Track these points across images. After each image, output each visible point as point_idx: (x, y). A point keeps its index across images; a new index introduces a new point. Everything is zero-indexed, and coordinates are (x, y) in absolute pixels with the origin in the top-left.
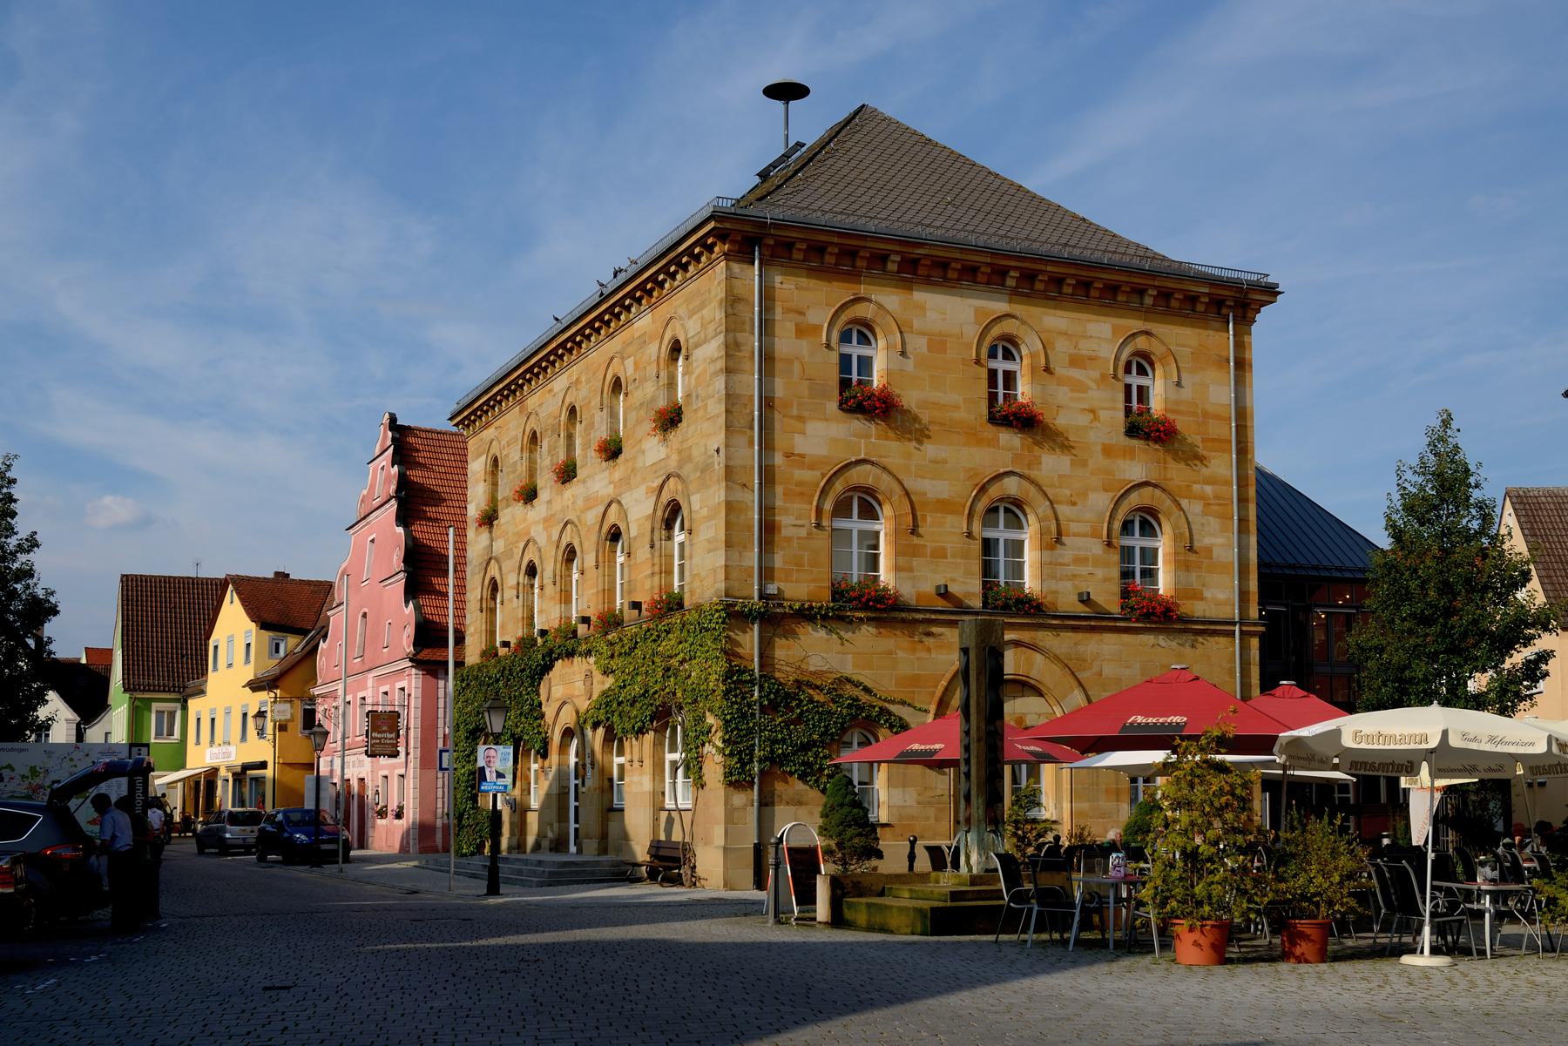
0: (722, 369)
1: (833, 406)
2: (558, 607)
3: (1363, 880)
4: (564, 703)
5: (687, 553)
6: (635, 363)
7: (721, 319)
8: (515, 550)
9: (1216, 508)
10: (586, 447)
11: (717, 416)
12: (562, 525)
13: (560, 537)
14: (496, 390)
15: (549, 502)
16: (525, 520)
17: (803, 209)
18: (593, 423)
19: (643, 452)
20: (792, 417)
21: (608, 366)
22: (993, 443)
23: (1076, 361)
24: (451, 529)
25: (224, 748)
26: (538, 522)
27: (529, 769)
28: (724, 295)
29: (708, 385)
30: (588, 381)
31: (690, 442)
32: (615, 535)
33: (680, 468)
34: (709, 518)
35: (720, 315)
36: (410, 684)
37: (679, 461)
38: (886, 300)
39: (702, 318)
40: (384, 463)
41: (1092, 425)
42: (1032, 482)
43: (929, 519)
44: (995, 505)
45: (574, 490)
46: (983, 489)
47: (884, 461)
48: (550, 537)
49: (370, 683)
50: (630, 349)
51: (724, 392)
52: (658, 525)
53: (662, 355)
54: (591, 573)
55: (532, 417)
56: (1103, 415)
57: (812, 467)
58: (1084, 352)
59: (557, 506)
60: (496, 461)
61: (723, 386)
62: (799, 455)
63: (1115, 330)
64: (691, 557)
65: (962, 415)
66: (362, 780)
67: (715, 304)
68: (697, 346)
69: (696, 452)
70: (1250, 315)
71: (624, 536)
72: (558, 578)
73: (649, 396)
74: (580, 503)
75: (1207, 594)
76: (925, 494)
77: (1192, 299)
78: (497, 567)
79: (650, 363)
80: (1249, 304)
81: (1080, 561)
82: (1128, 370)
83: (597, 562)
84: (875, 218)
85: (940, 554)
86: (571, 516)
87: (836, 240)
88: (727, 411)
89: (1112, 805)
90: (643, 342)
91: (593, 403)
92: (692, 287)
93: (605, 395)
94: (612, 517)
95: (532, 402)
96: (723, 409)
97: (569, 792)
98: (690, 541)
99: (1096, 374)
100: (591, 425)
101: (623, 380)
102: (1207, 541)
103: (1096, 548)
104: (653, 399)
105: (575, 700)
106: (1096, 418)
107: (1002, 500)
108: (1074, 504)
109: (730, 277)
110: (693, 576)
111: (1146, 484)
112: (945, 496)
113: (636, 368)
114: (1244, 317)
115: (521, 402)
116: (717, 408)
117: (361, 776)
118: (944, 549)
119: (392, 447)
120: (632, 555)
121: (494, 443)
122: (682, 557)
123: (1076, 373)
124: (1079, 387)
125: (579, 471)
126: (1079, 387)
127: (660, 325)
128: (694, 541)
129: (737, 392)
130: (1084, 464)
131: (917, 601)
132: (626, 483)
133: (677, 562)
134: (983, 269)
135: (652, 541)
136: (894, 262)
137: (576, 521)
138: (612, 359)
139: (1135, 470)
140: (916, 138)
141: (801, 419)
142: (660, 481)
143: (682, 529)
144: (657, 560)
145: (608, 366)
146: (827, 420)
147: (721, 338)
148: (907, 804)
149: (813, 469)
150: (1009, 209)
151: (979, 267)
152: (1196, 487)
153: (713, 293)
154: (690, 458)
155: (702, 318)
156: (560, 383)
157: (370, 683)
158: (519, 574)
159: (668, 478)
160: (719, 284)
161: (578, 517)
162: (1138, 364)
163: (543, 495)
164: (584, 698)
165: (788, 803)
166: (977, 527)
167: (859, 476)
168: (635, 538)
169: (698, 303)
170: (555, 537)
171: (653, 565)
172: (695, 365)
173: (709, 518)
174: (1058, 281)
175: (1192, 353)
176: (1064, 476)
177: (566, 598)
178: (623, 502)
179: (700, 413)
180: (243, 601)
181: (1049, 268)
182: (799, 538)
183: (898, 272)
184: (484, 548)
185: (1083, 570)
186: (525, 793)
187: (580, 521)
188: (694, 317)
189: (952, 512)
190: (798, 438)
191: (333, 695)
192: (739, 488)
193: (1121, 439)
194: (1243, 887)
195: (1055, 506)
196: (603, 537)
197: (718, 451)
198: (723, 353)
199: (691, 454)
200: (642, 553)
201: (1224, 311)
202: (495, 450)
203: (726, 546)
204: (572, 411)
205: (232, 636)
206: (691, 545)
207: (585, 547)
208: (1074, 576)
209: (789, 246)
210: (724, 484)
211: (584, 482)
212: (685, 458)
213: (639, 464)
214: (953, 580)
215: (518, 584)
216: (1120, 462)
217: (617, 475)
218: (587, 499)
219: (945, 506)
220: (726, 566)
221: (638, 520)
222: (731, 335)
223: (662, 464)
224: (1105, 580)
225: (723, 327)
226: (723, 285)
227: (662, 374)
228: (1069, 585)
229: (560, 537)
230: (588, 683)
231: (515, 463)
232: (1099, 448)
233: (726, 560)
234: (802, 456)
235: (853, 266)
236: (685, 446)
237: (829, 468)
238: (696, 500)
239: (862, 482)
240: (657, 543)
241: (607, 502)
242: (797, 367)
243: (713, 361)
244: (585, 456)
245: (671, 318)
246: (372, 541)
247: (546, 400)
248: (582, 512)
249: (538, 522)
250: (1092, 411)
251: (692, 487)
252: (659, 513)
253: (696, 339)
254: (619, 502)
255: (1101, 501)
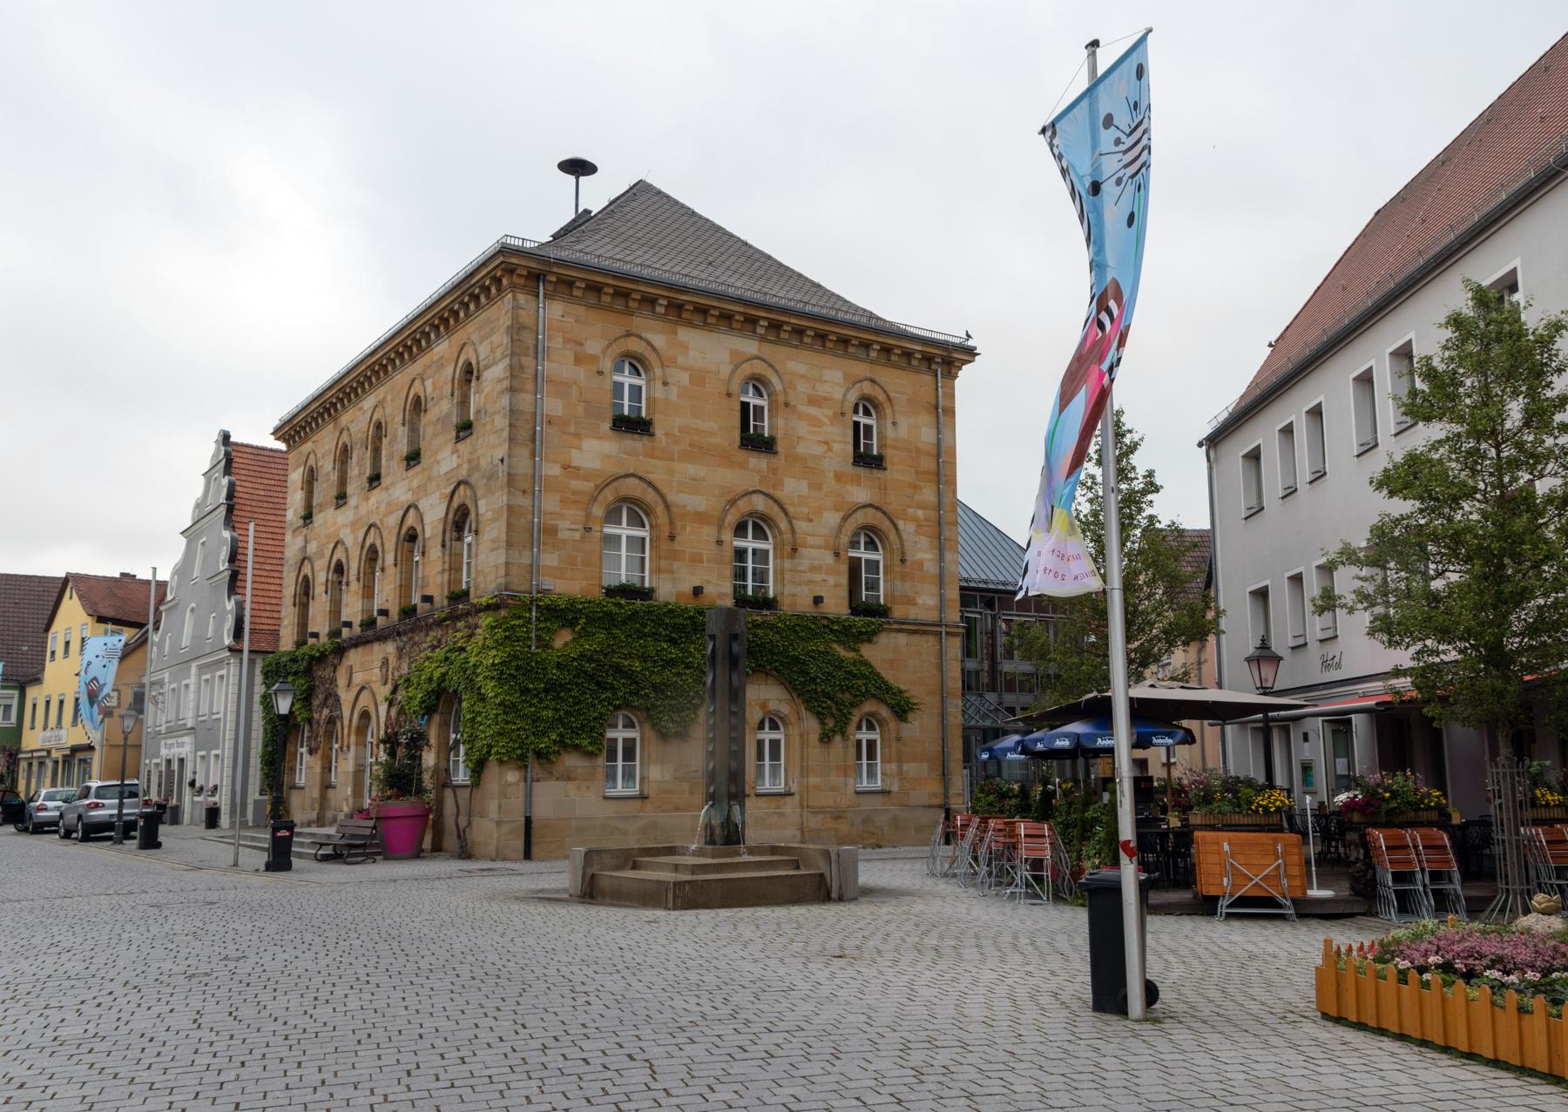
0: (506, 389)
1: (606, 426)
2: (360, 601)
3: (1473, 655)
4: (363, 688)
5: (473, 552)
6: (433, 384)
7: (507, 344)
8: (326, 551)
9: (927, 529)
10: (391, 457)
11: (502, 430)
12: (365, 529)
13: (365, 539)
14: (313, 407)
15: (357, 507)
16: (335, 523)
17: (587, 254)
18: (396, 437)
19: (438, 462)
20: (569, 434)
21: (410, 387)
22: (743, 466)
23: (814, 401)
24: (252, 526)
25: (56, 732)
26: (346, 525)
27: (331, 749)
28: (510, 322)
29: (496, 402)
30: (393, 400)
31: (479, 453)
32: (412, 537)
33: (469, 476)
34: (493, 520)
35: (506, 340)
36: (228, 671)
37: (469, 470)
38: (656, 335)
39: (492, 343)
40: (217, 475)
41: (827, 455)
42: (776, 501)
43: (688, 529)
44: (745, 519)
45: (376, 496)
46: (733, 502)
47: (650, 477)
48: (356, 538)
49: (194, 670)
50: (430, 371)
51: (508, 408)
52: (449, 528)
53: (457, 376)
54: (391, 570)
55: (345, 433)
56: (836, 447)
57: (586, 478)
58: (820, 393)
59: (363, 510)
60: (312, 470)
61: (508, 402)
62: (575, 467)
63: (846, 376)
64: (477, 555)
65: (717, 440)
66: (181, 761)
67: (502, 330)
68: (487, 367)
69: (484, 462)
70: (953, 371)
71: (420, 538)
72: (362, 575)
73: (444, 412)
74: (383, 508)
75: (920, 601)
76: (685, 506)
77: (908, 354)
78: (309, 567)
79: (446, 383)
80: (953, 362)
81: (815, 569)
82: (856, 411)
83: (396, 560)
84: (649, 266)
85: (696, 559)
86: (375, 519)
87: (611, 282)
88: (511, 425)
89: (841, 780)
90: (440, 365)
91: (397, 419)
92: (483, 316)
93: (407, 412)
94: (411, 519)
95: (345, 419)
96: (507, 423)
97: (364, 771)
98: (477, 540)
99: (830, 413)
100: (394, 439)
101: (423, 399)
102: (919, 556)
103: (829, 559)
104: (448, 415)
105: (373, 685)
106: (830, 449)
107: (750, 514)
108: (811, 521)
109: (516, 307)
110: (477, 572)
111: (871, 506)
112: (702, 509)
113: (434, 389)
114: (950, 373)
115: (335, 419)
116: (501, 422)
117: (181, 756)
118: (701, 554)
119: (224, 460)
120: (426, 555)
121: (312, 456)
122: (469, 557)
123: (813, 411)
124: (815, 422)
125: (383, 480)
126: (815, 422)
127: (455, 350)
128: (480, 541)
129: (521, 408)
130: (819, 487)
131: (677, 599)
132: (422, 489)
133: (465, 560)
134: (737, 317)
135: (444, 541)
136: (661, 305)
137: (378, 523)
138: (413, 380)
139: (861, 495)
140: (682, 211)
141: (577, 436)
142: (451, 488)
143: (470, 531)
144: (447, 558)
145: (410, 387)
146: (600, 438)
147: (506, 361)
148: (666, 778)
149: (588, 481)
150: (761, 273)
151: (734, 316)
152: (910, 511)
153: (501, 321)
154: (478, 467)
155: (492, 343)
156: (368, 403)
157: (194, 670)
158: (328, 572)
159: (459, 484)
160: (506, 313)
161: (381, 520)
162: (864, 406)
163: (352, 501)
164: (380, 683)
165: (558, 779)
166: (727, 536)
167: (632, 487)
168: (429, 538)
169: (488, 330)
170: (361, 539)
171: (444, 563)
172: (484, 384)
173: (493, 520)
174: (799, 332)
175: (908, 400)
176: (802, 496)
177: (368, 592)
178: (420, 506)
179: (488, 427)
180: (81, 597)
181: (793, 321)
182: (574, 541)
183: (665, 314)
184: (299, 549)
185: (818, 577)
186: (326, 771)
187: (382, 524)
188: (485, 343)
189: (708, 523)
190: (575, 453)
191: (161, 683)
192: (520, 494)
193: (847, 467)
194: (483, 691)
195: (794, 522)
196: (402, 537)
197: (502, 460)
198: (508, 374)
199: (479, 464)
200: (435, 552)
201: (934, 367)
202: (311, 462)
203: (507, 545)
204: (379, 426)
205: (70, 629)
206: (477, 544)
207: (386, 546)
208: (811, 582)
209: (570, 284)
210: (506, 490)
211: (387, 489)
212: (474, 466)
213: (435, 473)
214: (708, 582)
215: (327, 580)
216: (849, 487)
217: (415, 484)
218: (389, 504)
219: (701, 518)
220: (507, 564)
221: (432, 523)
222: (516, 358)
223: (454, 473)
224: (836, 586)
225: (509, 351)
226: (510, 314)
227: (456, 393)
228: (805, 589)
229: (365, 539)
230: (384, 670)
231: (328, 474)
232: (832, 474)
233: (507, 557)
234: (578, 469)
235: (627, 306)
236: (474, 456)
237: (602, 480)
238: (482, 503)
239: (631, 493)
240: (448, 543)
241: (406, 507)
242: (574, 390)
243: (500, 381)
244: (388, 467)
245: (465, 344)
246: (203, 544)
247: (357, 419)
248: (385, 516)
249: (346, 525)
250: (827, 443)
251: (479, 493)
252: (451, 516)
253: (486, 361)
254: (416, 508)
255: (832, 518)
